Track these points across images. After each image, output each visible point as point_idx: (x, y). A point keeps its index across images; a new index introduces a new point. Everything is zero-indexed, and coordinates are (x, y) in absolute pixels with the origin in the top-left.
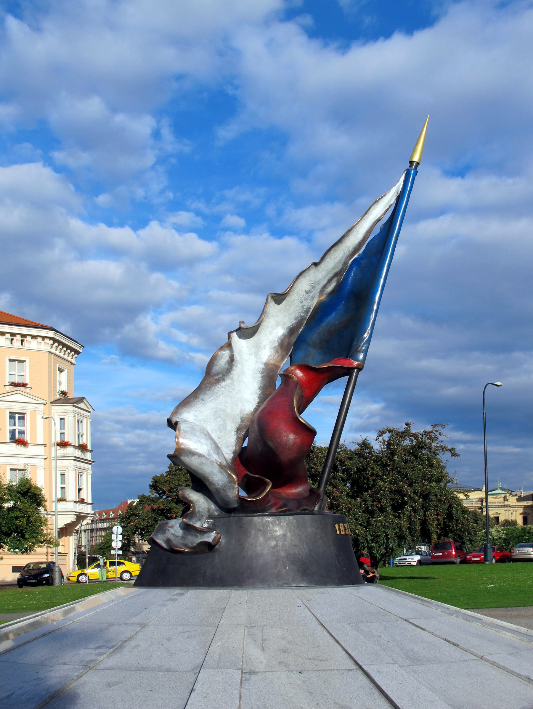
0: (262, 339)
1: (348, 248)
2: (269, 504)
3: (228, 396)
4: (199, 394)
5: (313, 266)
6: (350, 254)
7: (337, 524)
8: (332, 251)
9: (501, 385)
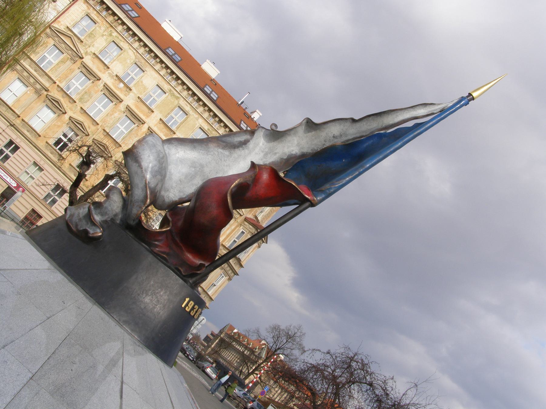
0: (279, 147)
5: (351, 120)
8: (371, 118)
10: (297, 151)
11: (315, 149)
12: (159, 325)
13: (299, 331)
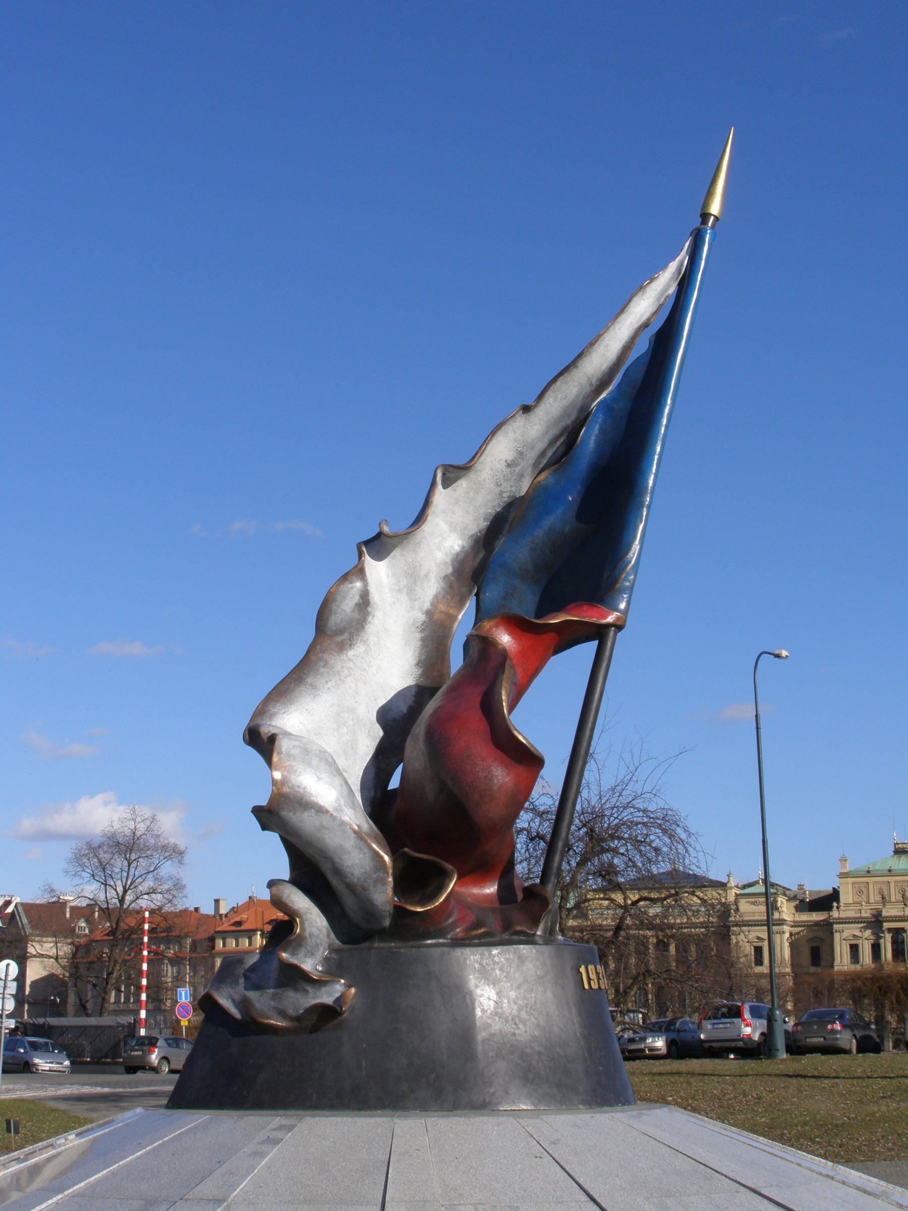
1: (589, 379)
2: (450, 921)
3: (361, 678)
4: (305, 674)
6: (593, 391)
7: (583, 967)
8: (558, 383)
9: (787, 656)
10: (460, 542)
11: (490, 513)
12: (586, 1054)
13: (139, 819)
